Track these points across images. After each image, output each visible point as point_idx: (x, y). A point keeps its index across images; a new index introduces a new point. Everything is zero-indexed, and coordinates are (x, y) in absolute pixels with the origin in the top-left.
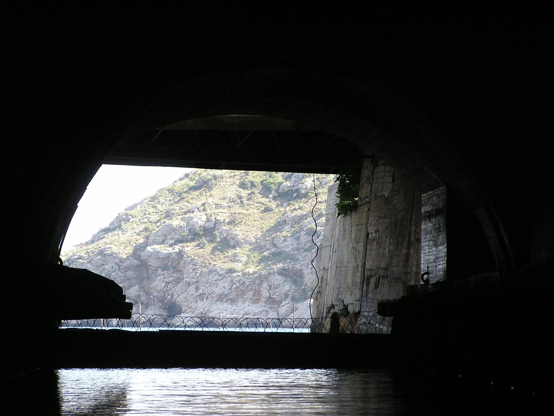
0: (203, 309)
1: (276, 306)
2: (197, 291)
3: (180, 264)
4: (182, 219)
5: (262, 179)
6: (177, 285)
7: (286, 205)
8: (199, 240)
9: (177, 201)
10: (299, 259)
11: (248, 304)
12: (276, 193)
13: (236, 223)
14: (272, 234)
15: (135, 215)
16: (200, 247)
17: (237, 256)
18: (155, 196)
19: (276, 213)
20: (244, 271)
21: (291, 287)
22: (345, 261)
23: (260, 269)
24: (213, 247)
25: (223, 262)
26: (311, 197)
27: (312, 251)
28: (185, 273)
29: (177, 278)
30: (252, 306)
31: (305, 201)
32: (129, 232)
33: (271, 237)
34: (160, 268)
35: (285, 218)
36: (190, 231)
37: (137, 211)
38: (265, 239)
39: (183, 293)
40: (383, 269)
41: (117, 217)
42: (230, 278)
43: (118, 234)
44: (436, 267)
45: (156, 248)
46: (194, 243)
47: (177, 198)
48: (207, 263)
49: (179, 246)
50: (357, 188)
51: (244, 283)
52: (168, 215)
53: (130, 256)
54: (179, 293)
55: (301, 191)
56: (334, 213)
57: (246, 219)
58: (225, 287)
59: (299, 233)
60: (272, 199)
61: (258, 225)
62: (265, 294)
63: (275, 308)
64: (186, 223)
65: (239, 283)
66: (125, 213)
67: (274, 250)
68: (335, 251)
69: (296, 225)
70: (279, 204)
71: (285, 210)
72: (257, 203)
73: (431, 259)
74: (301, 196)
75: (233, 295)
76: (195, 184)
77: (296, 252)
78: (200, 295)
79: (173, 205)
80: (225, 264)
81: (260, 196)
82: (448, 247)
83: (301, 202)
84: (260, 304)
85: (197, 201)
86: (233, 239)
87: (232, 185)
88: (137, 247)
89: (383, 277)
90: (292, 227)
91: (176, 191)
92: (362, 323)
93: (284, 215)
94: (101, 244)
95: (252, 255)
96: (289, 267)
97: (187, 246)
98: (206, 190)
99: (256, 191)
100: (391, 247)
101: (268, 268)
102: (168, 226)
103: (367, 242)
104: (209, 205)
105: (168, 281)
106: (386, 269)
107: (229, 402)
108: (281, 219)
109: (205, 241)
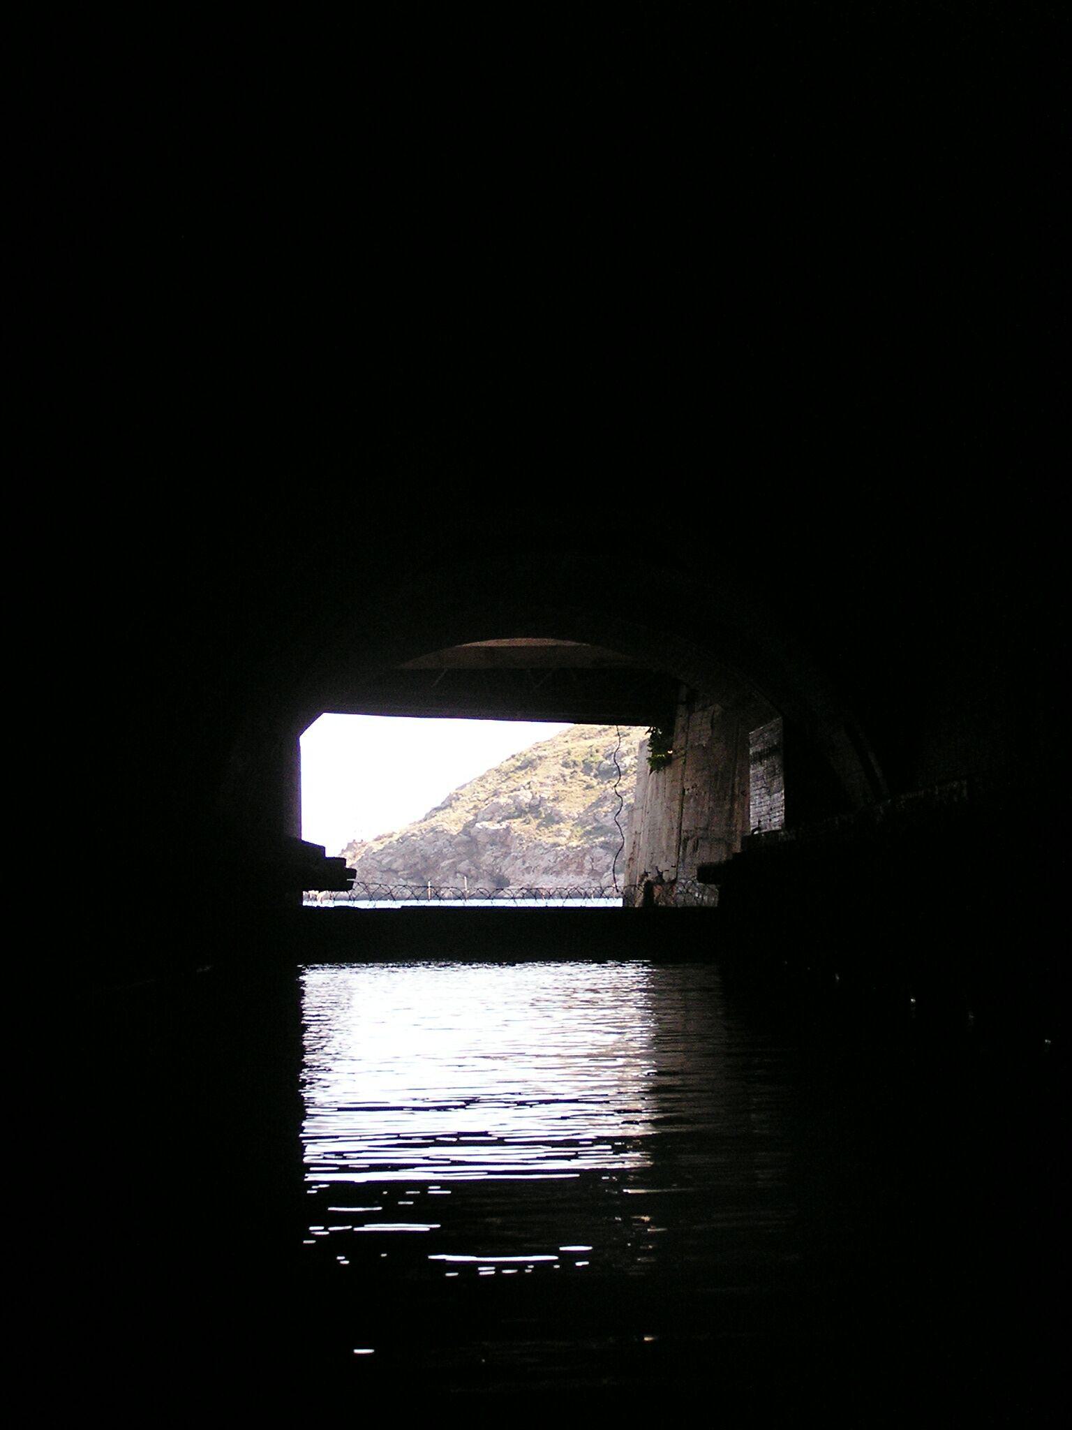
1: (598, 878)
2: (523, 864)
36: (516, 808)
44: (770, 820)
46: (521, 820)
51: (568, 856)
52: (496, 794)
53: (460, 832)
62: (588, 866)
72: (580, 781)
75: (558, 868)
82: (785, 794)
89: (701, 838)
90: (612, 803)
94: (433, 822)
95: (575, 831)
100: (711, 804)
103: (683, 800)
106: (706, 829)
109: (531, 818)
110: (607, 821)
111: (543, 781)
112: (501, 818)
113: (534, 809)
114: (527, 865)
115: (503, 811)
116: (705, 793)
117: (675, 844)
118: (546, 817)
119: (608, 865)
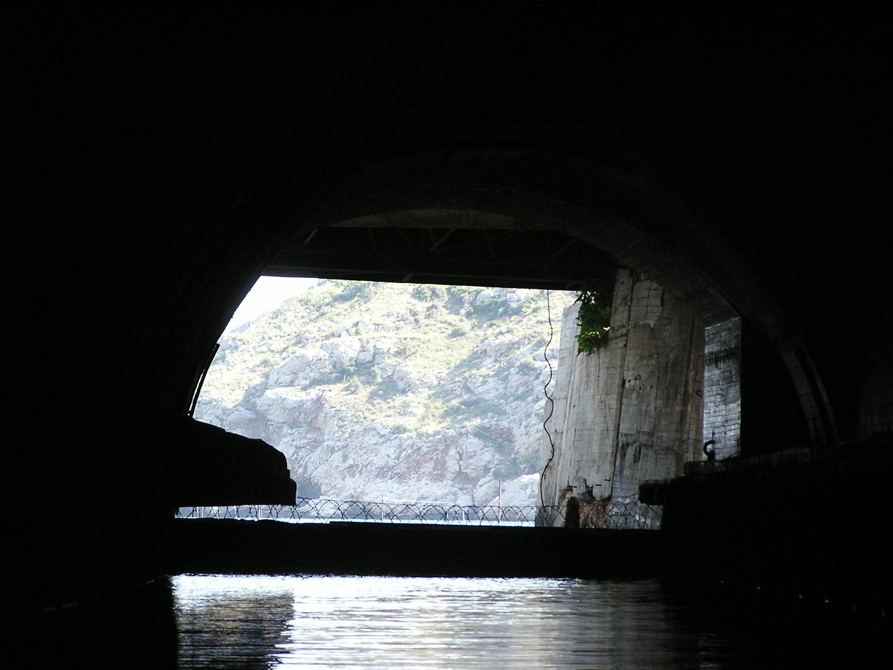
0: (354, 489)
2: (344, 461)
3: (319, 418)
4: (321, 348)
6: (314, 452)
7: (487, 326)
8: (349, 381)
9: (314, 319)
10: (507, 411)
11: (426, 482)
12: (471, 308)
13: (408, 354)
14: (464, 372)
15: (248, 340)
17: (408, 406)
18: (280, 310)
19: (471, 339)
20: (419, 430)
21: (493, 457)
22: (589, 420)
23: (445, 427)
24: (370, 392)
25: (386, 416)
26: (527, 313)
27: (528, 399)
28: (326, 432)
29: (313, 440)
30: (432, 485)
31: (517, 320)
33: (462, 377)
34: (286, 425)
35: (486, 346)
36: (334, 366)
37: (251, 333)
38: (452, 379)
39: (323, 463)
40: (645, 434)
42: (397, 442)
43: (220, 369)
44: (725, 434)
45: (281, 393)
47: (313, 314)
48: (361, 417)
49: (316, 389)
50: (608, 312)
51: (419, 449)
52: (300, 341)
53: (240, 405)
54: (316, 464)
55: (511, 304)
56: (572, 349)
57: (423, 347)
58: (390, 455)
59: (507, 371)
60: (464, 317)
61: (443, 357)
62: (453, 466)
63: (468, 489)
64: (328, 353)
65: (411, 449)
66: (232, 337)
67: (467, 396)
68: (574, 406)
69: (503, 357)
70: (476, 324)
71: (485, 334)
72: (441, 322)
73: (718, 422)
74: (511, 312)
75: (402, 468)
76: (343, 291)
77: (501, 401)
78: (350, 467)
79: (308, 324)
80: (389, 418)
82: (743, 405)
83: (511, 321)
84: (445, 482)
85: (347, 318)
87: (401, 294)
88: (251, 391)
89: (645, 445)
90: (496, 361)
91: (313, 302)
92: (614, 513)
93: (483, 342)
95: (432, 405)
96: (491, 424)
98: (360, 302)
100: (659, 402)
101: (458, 426)
102: (299, 358)
103: (622, 394)
104: (365, 325)
105: (300, 444)
106: (651, 434)
108: (478, 348)
109: (359, 383)
110: (488, 392)
111: (380, 321)
112: (307, 382)
114: (350, 462)
116: (652, 387)
117: (610, 451)
118: (383, 383)
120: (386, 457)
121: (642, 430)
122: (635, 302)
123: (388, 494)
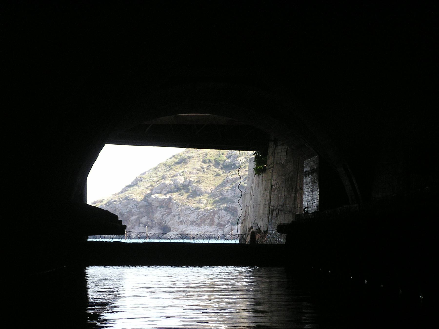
2: (179, 219)
5: (215, 158)
9: (169, 170)
11: (207, 226)
16: (180, 195)
20: (205, 209)
21: (231, 217)
32: (142, 187)
36: (175, 187)
38: (216, 191)
41: (135, 179)
42: (197, 212)
44: (312, 204)
46: (178, 193)
51: (205, 215)
52: (163, 178)
53: (142, 200)
60: (220, 169)
62: (216, 221)
70: (224, 171)
72: (212, 171)
75: (199, 221)
78: (181, 221)
81: (214, 167)
83: (236, 171)
84: (214, 226)
86: (199, 191)
89: (280, 210)
90: (231, 184)
91: (168, 164)
93: (227, 178)
94: (126, 194)
95: (209, 200)
97: (174, 195)
99: (211, 164)
100: (286, 193)
106: (283, 206)
107: (104, 319)
109: (183, 192)
110: (228, 195)
111: (191, 171)
113: (185, 187)
114: (181, 220)
115: (167, 188)
116: (283, 187)
119: (228, 221)
120: (193, 218)
121: (279, 204)
122: (276, 155)
123: (194, 230)
